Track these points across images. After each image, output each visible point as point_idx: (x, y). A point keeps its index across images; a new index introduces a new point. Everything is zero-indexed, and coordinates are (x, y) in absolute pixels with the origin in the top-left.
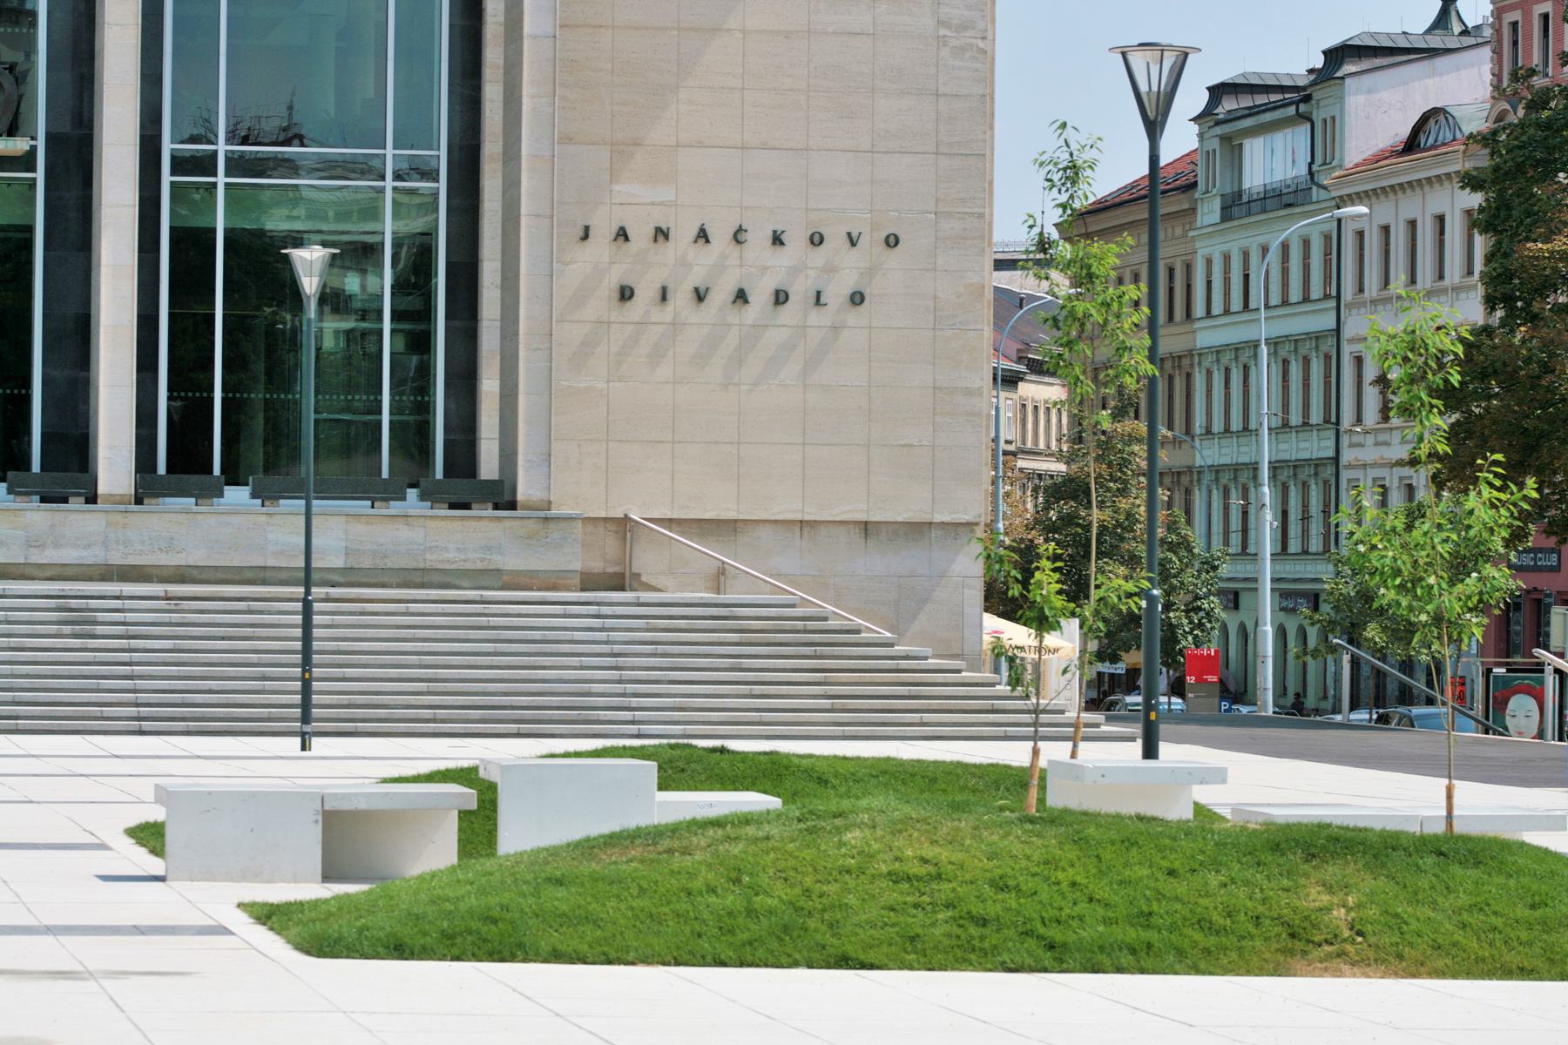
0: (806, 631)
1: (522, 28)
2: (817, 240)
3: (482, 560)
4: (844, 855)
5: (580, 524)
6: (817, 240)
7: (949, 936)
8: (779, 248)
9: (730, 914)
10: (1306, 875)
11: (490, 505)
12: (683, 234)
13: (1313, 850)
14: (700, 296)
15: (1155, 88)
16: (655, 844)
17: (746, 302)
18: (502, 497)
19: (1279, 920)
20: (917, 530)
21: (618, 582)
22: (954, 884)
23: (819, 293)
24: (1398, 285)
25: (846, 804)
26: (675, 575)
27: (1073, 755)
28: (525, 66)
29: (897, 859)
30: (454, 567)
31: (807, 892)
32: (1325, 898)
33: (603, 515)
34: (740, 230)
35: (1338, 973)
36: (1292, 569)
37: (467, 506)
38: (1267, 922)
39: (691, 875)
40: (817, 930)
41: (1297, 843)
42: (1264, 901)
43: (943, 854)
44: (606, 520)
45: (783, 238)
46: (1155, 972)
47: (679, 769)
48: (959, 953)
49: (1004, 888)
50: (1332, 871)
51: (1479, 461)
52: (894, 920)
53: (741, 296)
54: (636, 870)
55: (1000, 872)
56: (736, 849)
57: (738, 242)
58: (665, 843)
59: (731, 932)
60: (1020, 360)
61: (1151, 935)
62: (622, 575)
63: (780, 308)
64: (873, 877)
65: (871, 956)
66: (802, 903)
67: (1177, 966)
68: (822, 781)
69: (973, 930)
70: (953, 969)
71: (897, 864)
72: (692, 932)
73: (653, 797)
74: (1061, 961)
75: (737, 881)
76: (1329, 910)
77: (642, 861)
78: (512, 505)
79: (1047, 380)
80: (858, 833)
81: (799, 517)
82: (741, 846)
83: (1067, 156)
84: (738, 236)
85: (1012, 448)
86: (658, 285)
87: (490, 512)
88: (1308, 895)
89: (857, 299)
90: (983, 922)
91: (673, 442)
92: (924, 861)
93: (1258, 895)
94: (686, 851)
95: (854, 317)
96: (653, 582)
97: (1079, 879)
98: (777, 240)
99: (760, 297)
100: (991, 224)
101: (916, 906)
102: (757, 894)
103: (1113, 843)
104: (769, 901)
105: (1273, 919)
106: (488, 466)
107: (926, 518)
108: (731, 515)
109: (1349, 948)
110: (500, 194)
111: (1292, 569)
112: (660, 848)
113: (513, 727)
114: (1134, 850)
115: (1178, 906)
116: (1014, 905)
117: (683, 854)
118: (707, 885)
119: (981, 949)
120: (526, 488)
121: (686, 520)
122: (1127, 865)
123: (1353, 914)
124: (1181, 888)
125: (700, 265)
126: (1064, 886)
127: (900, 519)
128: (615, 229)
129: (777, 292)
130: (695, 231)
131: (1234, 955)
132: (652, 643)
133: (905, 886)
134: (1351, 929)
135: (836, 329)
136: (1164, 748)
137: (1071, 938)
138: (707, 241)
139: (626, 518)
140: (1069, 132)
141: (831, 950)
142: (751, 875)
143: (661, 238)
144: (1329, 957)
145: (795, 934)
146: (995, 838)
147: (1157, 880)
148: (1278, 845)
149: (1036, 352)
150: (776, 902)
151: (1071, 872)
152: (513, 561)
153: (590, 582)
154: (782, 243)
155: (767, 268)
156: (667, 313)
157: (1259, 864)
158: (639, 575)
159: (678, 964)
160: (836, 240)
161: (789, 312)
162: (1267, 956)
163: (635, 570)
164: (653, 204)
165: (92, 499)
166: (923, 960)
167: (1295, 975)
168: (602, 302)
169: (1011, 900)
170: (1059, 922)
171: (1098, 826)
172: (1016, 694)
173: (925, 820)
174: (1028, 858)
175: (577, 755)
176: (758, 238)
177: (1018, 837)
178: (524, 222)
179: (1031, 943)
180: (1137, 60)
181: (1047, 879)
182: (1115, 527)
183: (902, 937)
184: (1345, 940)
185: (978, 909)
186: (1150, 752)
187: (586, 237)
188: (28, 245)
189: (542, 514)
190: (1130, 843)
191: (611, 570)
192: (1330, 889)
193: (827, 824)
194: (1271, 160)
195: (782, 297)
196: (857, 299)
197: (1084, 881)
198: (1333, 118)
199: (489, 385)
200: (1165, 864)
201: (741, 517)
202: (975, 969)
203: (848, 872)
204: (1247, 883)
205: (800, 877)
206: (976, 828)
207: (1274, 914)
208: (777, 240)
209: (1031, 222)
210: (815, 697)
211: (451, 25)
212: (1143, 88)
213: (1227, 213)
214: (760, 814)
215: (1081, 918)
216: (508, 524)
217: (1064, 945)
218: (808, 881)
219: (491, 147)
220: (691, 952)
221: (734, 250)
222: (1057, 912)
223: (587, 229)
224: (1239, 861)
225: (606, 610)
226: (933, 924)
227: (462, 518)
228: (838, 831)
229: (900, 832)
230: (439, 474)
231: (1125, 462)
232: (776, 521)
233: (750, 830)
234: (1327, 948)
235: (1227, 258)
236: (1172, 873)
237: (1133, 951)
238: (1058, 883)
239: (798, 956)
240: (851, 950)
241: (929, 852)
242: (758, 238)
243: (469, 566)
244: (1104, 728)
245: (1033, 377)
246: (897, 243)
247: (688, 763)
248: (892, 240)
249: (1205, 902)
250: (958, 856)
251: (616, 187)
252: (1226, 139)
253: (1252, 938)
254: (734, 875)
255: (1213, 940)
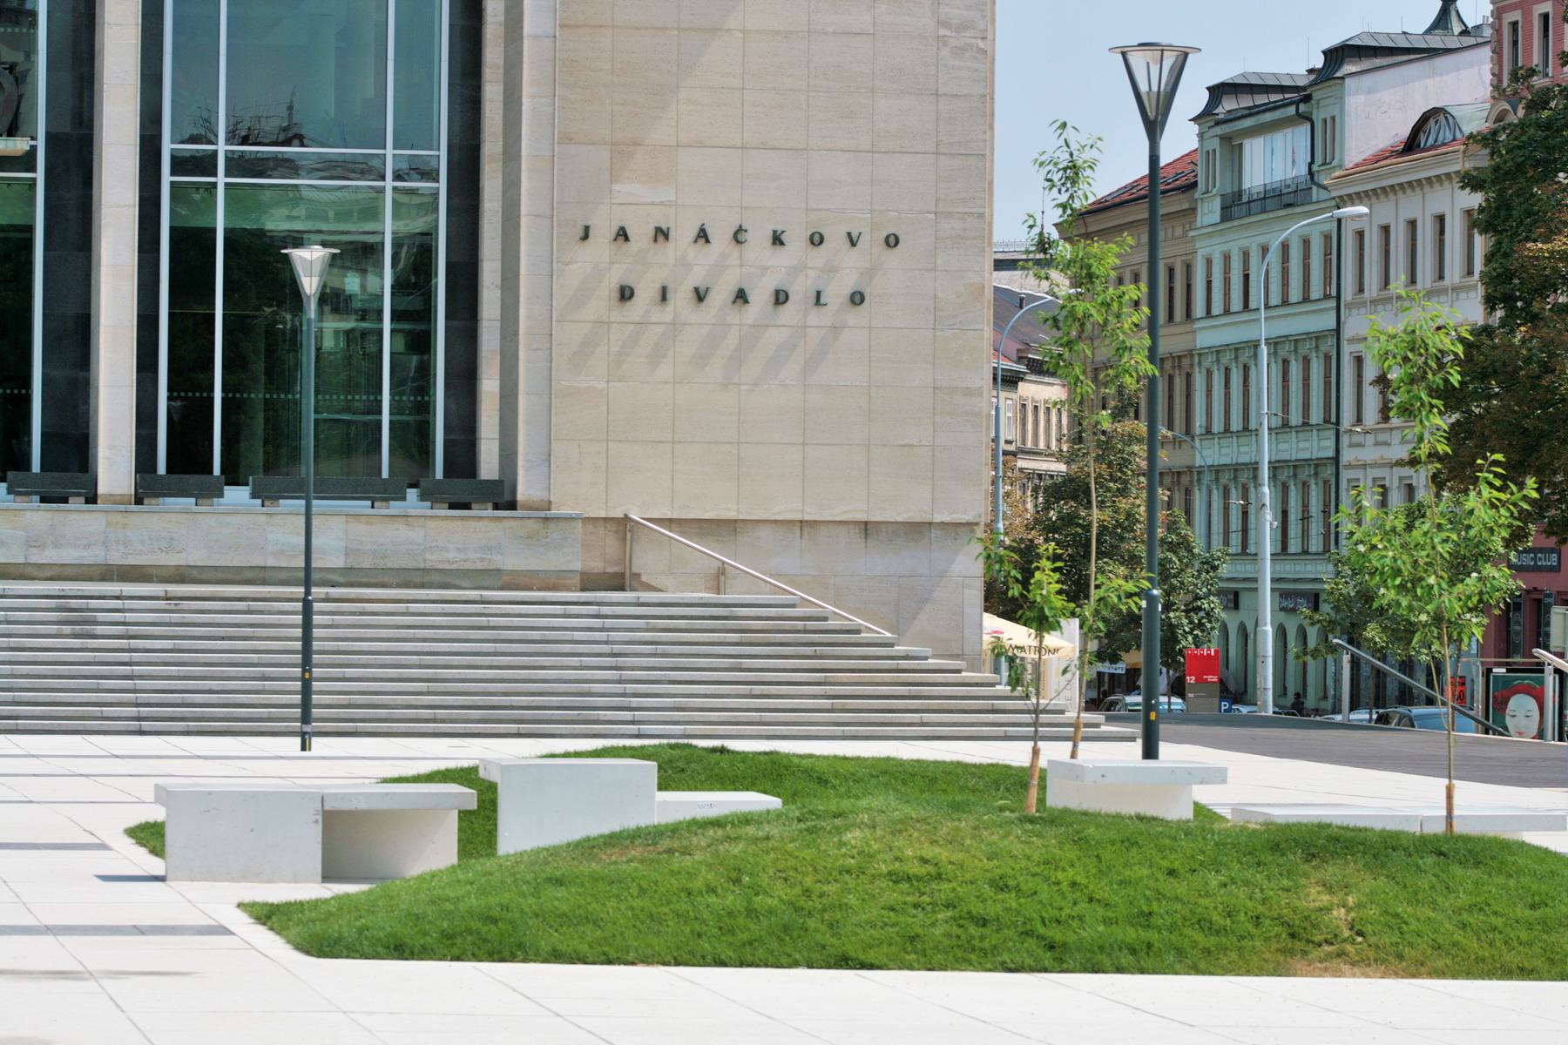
0: (806, 631)
1: (522, 28)
2: (817, 240)
3: (482, 560)
4: (844, 855)
5: (580, 524)
6: (817, 240)
7: (949, 936)
8: (779, 248)
9: (730, 914)
10: (1306, 875)
11: (490, 505)
12: (683, 234)
13: (1313, 850)
14: (700, 296)
15: (1155, 88)
16: (655, 844)
17: (746, 302)
18: (502, 497)
19: (1279, 920)
20: (917, 530)
21: (618, 582)
22: (954, 884)
23: (819, 293)
24: (1398, 285)
25: (846, 804)
26: (675, 575)
27: (1073, 755)
28: (525, 66)
29: (897, 859)
30: (454, 567)
31: (807, 892)
32: (1325, 898)
33: (603, 515)
34: (740, 230)
35: (1338, 973)
36: (1292, 569)
37: (467, 506)
38: (1267, 922)
39: (691, 875)
40: (817, 930)
41: (1297, 843)
42: (1264, 901)
43: (943, 854)
44: (606, 520)
45: (783, 238)
46: (1155, 972)
47: (679, 769)
48: (959, 953)
49: (1004, 888)
50: (1332, 871)
51: (1479, 461)
52: (894, 920)
53: (741, 296)
54: (636, 870)
55: (1000, 872)
56: (736, 849)
57: (738, 242)
58: (665, 843)
59: (731, 932)
60: (1020, 360)
61: (1151, 935)
62: (622, 575)
63: (780, 308)
64: (873, 877)
65: (871, 956)
66: (802, 903)
67: (1177, 966)
68: (822, 781)
69: (973, 930)
70: (953, 969)
71: (897, 864)
72: (692, 932)
73: (653, 797)
74: (1061, 961)
75: (737, 881)
76: (1329, 910)
77: (642, 861)
78: (512, 505)
79: (1047, 380)
80: (858, 833)
81: (799, 517)
82: (741, 846)
83: (1067, 156)
84: (738, 236)
85: (1012, 448)
86: (658, 285)
87: (490, 512)
88: (1308, 895)
89: (857, 299)
90: (983, 922)
91: (673, 442)
92: (924, 861)
93: (1258, 895)
94: (686, 851)
95: (854, 317)
96: (653, 582)
97: (1079, 879)
98: (777, 240)
99: (760, 297)
100: (991, 224)
101: (916, 906)
102: (757, 894)
103: (1113, 843)
104: (769, 901)
105: (1273, 919)
106: (488, 466)
107: (926, 518)
108: (731, 515)
109: (1349, 948)
110: (500, 194)
111: (1292, 569)
112: (660, 848)
113: (513, 727)
114: (1134, 850)
115: (1178, 906)
116: (1014, 905)
117: (683, 854)
118: (707, 885)
119: (981, 949)
120: (526, 488)
121: (686, 520)
122: (1127, 865)
123: (1353, 914)
124: (1181, 888)
125: (700, 265)
126: (1064, 886)
127: (900, 519)
128: (615, 229)
129: (777, 292)
130: (695, 231)
131: (1234, 955)
132: (652, 643)
133: (905, 886)
134: (1351, 929)
135: (836, 329)
136: (1164, 748)
137: (1071, 938)
138: (707, 241)
139: (626, 518)
140: (1069, 132)
141: (831, 950)
142: (751, 875)
143: (661, 238)
144: (1329, 957)
145: (795, 934)
146: (995, 838)
147: (1157, 880)
148: (1278, 845)
149: (1036, 352)
150: (776, 902)
151: (1071, 872)
152: (513, 561)
153: (590, 582)
154: (782, 243)
155: (767, 268)
156: (667, 313)
157: (1259, 864)
158: (639, 575)
159: (678, 964)
160: (836, 240)
161: (789, 312)
162: (1267, 956)
163: (635, 570)
164: (653, 204)
165: (92, 499)
166: (923, 960)
167: (1295, 975)
168: (602, 302)
169: (1011, 900)
170: (1059, 922)
171: (1098, 826)
172: (1016, 694)
173: (925, 820)
174: (1028, 858)
175: (577, 755)
176: (758, 238)
177: (1018, 837)
178: (524, 222)
179: (1031, 943)
180: (1137, 60)
181: (1047, 879)
182: (1115, 527)
183: (902, 937)
184: (1345, 940)
185: (978, 909)
186: (1150, 752)
187: (586, 237)
188: (28, 245)
189: (542, 514)
190: (1130, 843)
191: (611, 570)
192: (1330, 889)
193: (827, 824)
194: (1271, 160)
195: (782, 297)
196: (857, 299)
197: (1084, 881)
198: (1333, 118)
199: (489, 385)
200: (1165, 864)
201: (741, 517)
202: (975, 969)
203: (848, 872)
204: (1247, 883)
205: (800, 877)
206: (976, 828)
207: (1274, 914)
208: (777, 240)
209: (1031, 222)
210: (815, 697)
211: (451, 25)
212: (1143, 88)
213: (1227, 213)
214: (760, 814)
215: (1081, 918)
216: (508, 524)
217: (1064, 945)
218: (808, 881)
219: (491, 147)
220: (691, 952)
221: (734, 250)
222: (1057, 912)
223: (587, 229)
224: (1239, 861)
225: (606, 610)
226: (933, 924)
227: (462, 518)
228: (838, 831)
229: (900, 832)
230: (439, 474)
231: (1125, 462)
232: (776, 521)
233: (750, 830)
234: (1327, 948)
235: (1227, 258)
236: (1172, 873)
237: (1133, 951)
238: (1058, 883)
239: (798, 956)
240: (851, 950)
241: (929, 852)
242: (758, 238)
243: (469, 566)
244: (1104, 728)
245: (1033, 377)
246: (897, 243)
247: (688, 763)
248: (892, 240)
249: (1205, 902)
250: (958, 856)
251: (616, 187)
252: (1226, 139)
253: (1252, 938)
254: (734, 875)
255: (1213, 940)
